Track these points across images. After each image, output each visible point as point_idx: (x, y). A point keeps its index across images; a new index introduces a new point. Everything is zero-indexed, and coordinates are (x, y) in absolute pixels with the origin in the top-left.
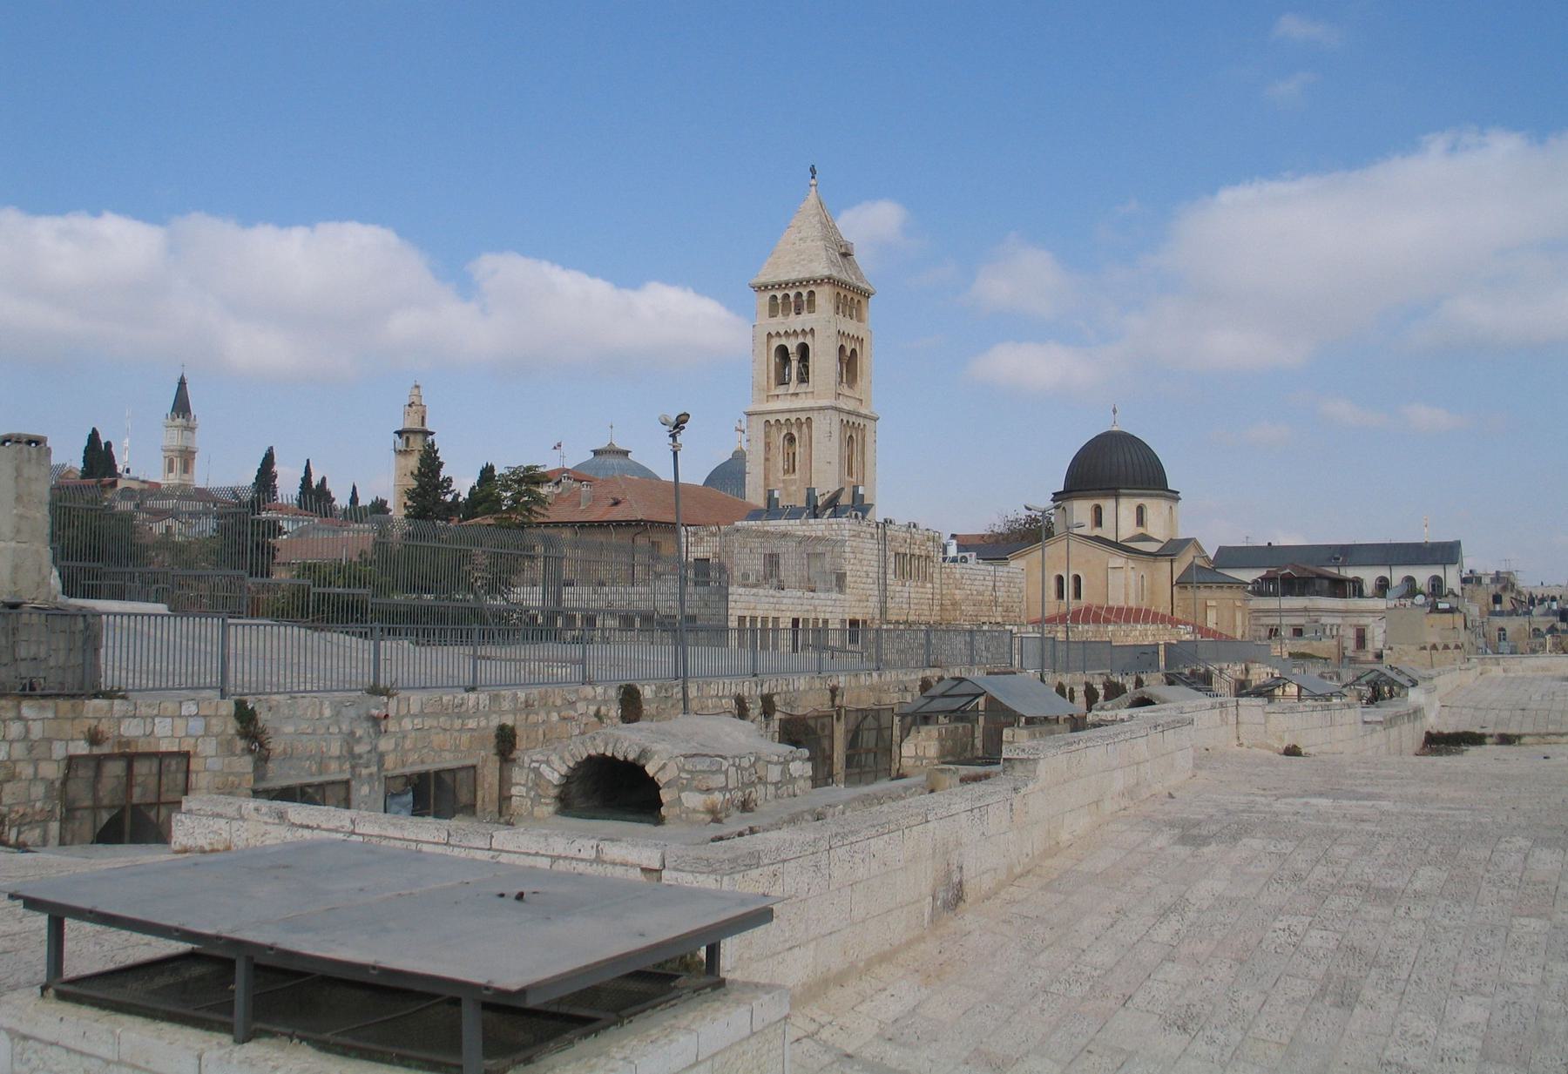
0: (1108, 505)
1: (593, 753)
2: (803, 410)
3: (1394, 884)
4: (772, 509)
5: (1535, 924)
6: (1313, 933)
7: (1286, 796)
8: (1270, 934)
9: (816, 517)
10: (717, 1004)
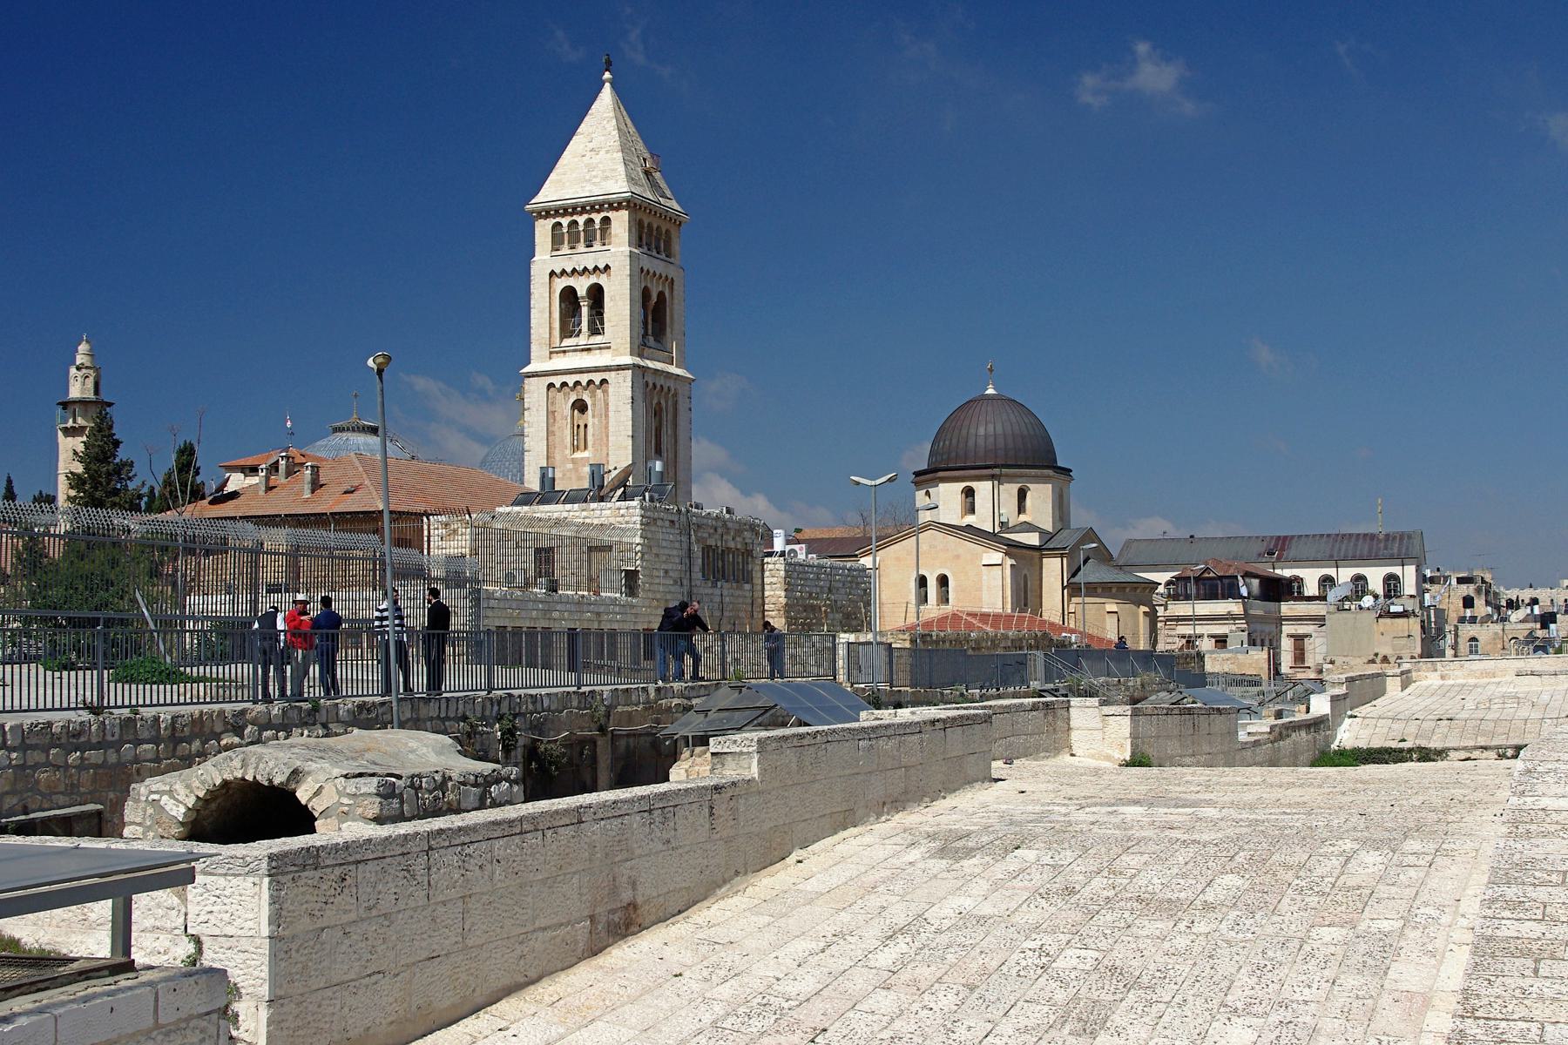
0: (983, 489)
1: (229, 777)
2: (597, 370)
3: (1183, 895)
4: (549, 493)
5: (1336, 933)
6: (1069, 952)
7: (1096, 805)
8: (1015, 957)
9: (602, 499)
10: (48, 948)
